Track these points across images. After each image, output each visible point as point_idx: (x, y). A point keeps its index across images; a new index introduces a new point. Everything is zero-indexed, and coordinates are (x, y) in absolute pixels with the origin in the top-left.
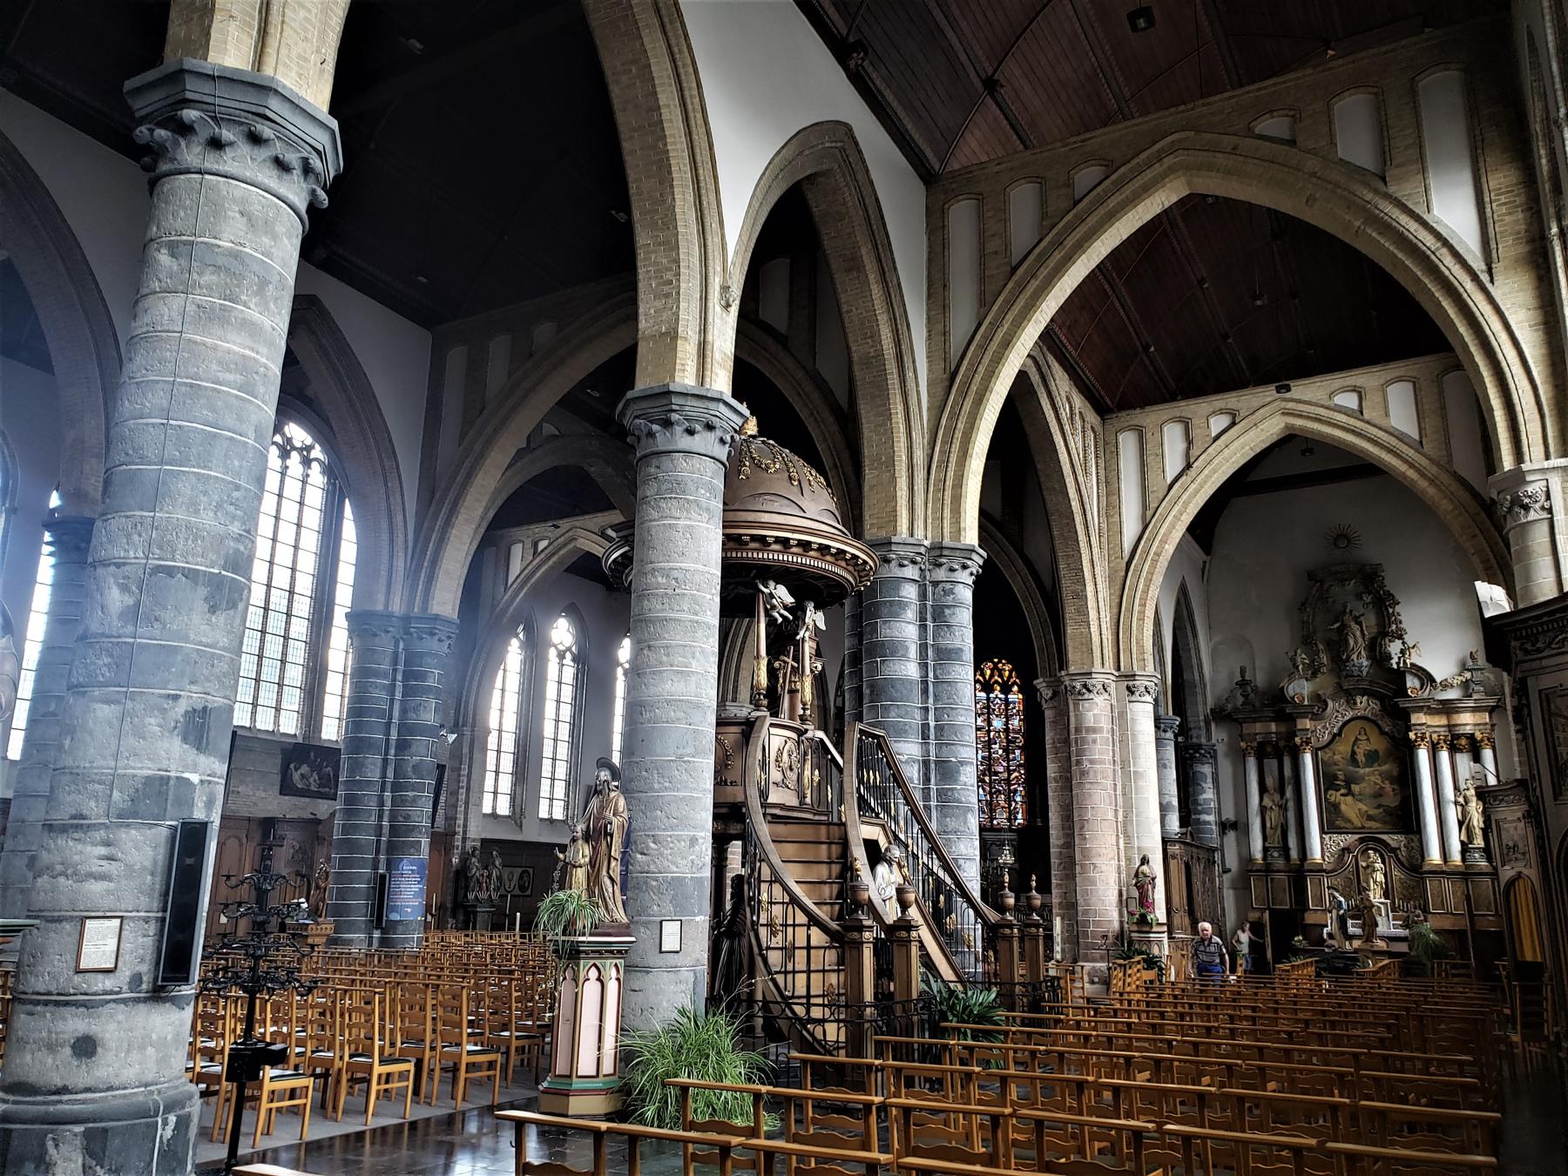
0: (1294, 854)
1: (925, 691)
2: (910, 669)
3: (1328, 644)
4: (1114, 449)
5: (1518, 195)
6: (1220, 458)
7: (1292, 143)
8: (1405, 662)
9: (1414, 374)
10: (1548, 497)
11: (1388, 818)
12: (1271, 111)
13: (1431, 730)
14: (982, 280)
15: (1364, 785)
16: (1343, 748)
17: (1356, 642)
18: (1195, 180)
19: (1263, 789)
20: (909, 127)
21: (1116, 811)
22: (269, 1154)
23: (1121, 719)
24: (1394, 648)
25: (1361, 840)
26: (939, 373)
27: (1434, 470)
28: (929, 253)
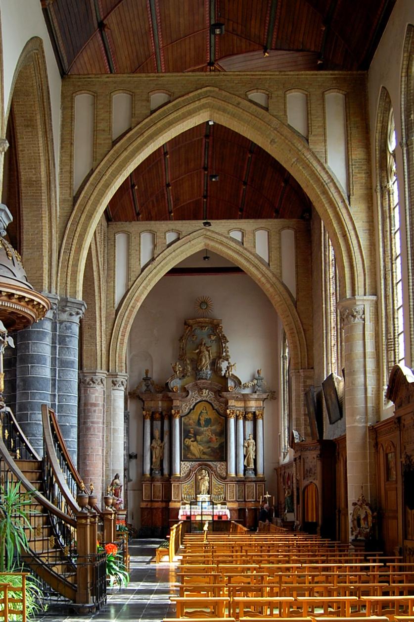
0: (166, 472)
1: (54, 385)
2: (45, 372)
3: (192, 360)
4: (113, 243)
5: (363, 165)
6: (170, 256)
7: (267, 109)
8: (229, 373)
9: (269, 228)
10: (364, 314)
11: (212, 454)
12: (257, 89)
13: (236, 409)
14: (95, 144)
15: (203, 436)
16: (194, 417)
17: (206, 361)
18: (215, 115)
19: (152, 437)
20: (60, 43)
21: (103, 450)
22: (407, 569)
23: (108, 399)
24: (224, 365)
25: (200, 465)
26: (67, 197)
27: (274, 279)
28: (63, 121)
